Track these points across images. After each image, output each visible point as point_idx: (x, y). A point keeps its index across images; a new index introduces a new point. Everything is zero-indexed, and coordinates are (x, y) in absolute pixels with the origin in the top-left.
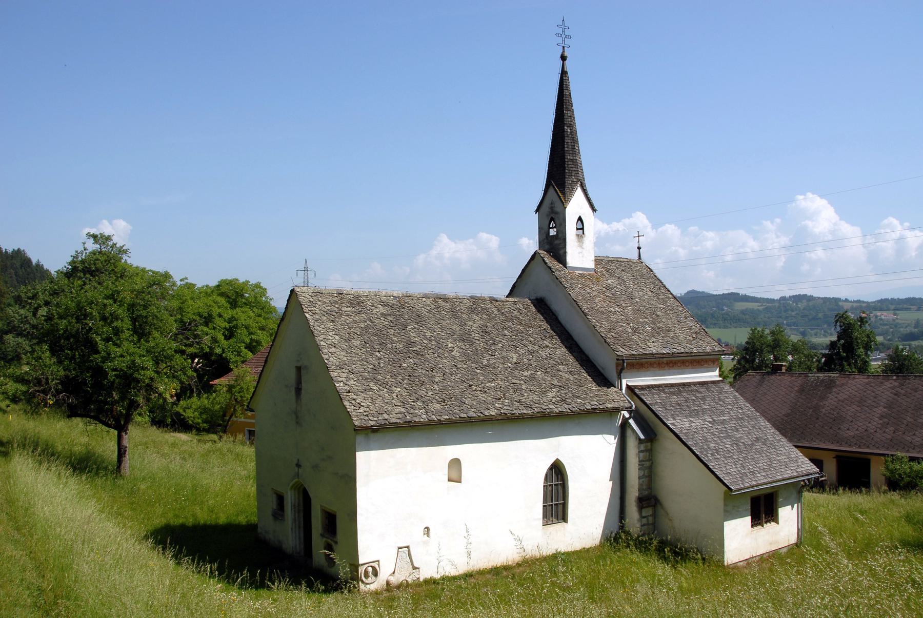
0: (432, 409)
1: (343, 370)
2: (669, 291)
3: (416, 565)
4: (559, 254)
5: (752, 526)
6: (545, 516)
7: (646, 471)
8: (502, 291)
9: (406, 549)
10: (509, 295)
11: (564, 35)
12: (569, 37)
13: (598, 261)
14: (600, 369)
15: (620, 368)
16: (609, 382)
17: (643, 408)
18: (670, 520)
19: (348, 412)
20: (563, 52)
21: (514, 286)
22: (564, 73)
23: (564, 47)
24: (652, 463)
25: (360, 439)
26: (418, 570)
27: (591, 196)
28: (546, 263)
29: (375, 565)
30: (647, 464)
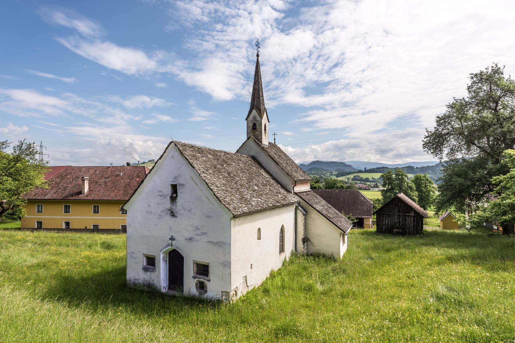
8: (234, 151)
18: (314, 246)
20: (258, 53)
23: (258, 51)
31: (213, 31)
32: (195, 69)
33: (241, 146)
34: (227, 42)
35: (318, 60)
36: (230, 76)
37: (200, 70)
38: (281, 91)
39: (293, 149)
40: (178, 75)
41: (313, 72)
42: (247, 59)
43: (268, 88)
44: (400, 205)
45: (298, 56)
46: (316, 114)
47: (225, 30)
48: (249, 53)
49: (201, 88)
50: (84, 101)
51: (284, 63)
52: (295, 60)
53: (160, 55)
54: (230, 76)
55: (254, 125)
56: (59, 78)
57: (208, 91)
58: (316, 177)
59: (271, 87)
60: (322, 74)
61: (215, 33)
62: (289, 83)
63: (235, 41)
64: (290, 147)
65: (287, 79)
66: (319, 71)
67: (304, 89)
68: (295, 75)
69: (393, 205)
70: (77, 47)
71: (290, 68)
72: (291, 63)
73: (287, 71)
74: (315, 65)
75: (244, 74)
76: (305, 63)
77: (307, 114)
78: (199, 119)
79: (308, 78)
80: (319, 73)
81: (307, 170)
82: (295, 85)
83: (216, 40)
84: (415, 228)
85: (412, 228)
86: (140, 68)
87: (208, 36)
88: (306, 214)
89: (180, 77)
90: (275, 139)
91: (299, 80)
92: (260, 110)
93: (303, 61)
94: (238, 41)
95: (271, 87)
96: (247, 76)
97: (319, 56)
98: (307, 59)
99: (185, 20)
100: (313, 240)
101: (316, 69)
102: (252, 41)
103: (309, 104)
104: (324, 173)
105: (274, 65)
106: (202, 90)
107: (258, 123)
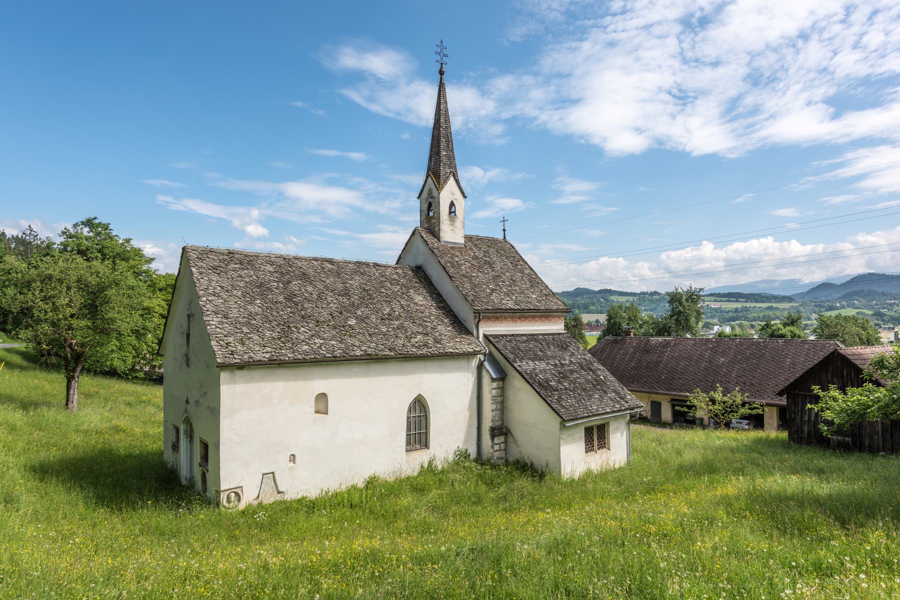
0: (300, 350)
1: (218, 316)
2: (526, 263)
3: (281, 489)
4: (435, 233)
5: (587, 452)
6: (408, 443)
7: (498, 405)
8: (392, 262)
9: (272, 475)
10: (397, 263)
11: (442, 53)
12: (446, 56)
13: (468, 238)
14: (462, 321)
15: (477, 320)
16: (467, 330)
17: (496, 354)
18: (518, 446)
19: (214, 351)
20: (442, 67)
21: (400, 258)
23: (442, 64)
25: (224, 376)
26: (283, 494)
27: (462, 185)
28: (422, 237)
29: (239, 491)
30: (500, 399)
31: (603, 17)
32: (567, 102)
33: (404, 249)
34: (633, 33)
35: (872, 24)
36: (643, 101)
37: (576, 102)
38: (765, 116)
39: (802, 247)
40: (536, 118)
41: (857, 55)
42: (680, 58)
43: (734, 113)
44: (847, 374)
45: (813, 27)
46: (866, 157)
47: (629, 9)
48: (685, 45)
49: (582, 137)
50: (380, 189)
51: (775, 50)
52: (804, 36)
53: (504, 84)
54: (643, 101)
55: (430, 205)
56: (345, 154)
57: (596, 141)
58: (864, 314)
59: (741, 110)
60: (883, 56)
61: (608, 19)
62: (789, 92)
63: (651, 25)
64: (794, 242)
65: (781, 85)
66: (875, 51)
67: (828, 101)
68: (803, 72)
69: (829, 374)
70: (371, 99)
71: (789, 58)
72: (794, 46)
73: (783, 66)
74: (861, 38)
75: (675, 91)
76: (830, 39)
77: (839, 160)
78: (574, 199)
79: (840, 73)
80: (874, 54)
81: (840, 298)
82: (804, 96)
83: (611, 32)
84: (888, 437)
85: (880, 435)
86: (468, 117)
87: (595, 29)
88: (502, 377)
89: (539, 122)
90: (504, 230)
91: (817, 82)
92: (439, 176)
93: (826, 35)
94: (660, 23)
95: (741, 110)
96: (682, 95)
97: (875, 13)
98: (837, 28)
99: (548, 8)
100: (519, 432)
101: (865, 47)
102: (692, 15)
103: (847, 135)
104: (891, 305)
105: (748, 58)
106: (583, 141)
107: (435, 202)
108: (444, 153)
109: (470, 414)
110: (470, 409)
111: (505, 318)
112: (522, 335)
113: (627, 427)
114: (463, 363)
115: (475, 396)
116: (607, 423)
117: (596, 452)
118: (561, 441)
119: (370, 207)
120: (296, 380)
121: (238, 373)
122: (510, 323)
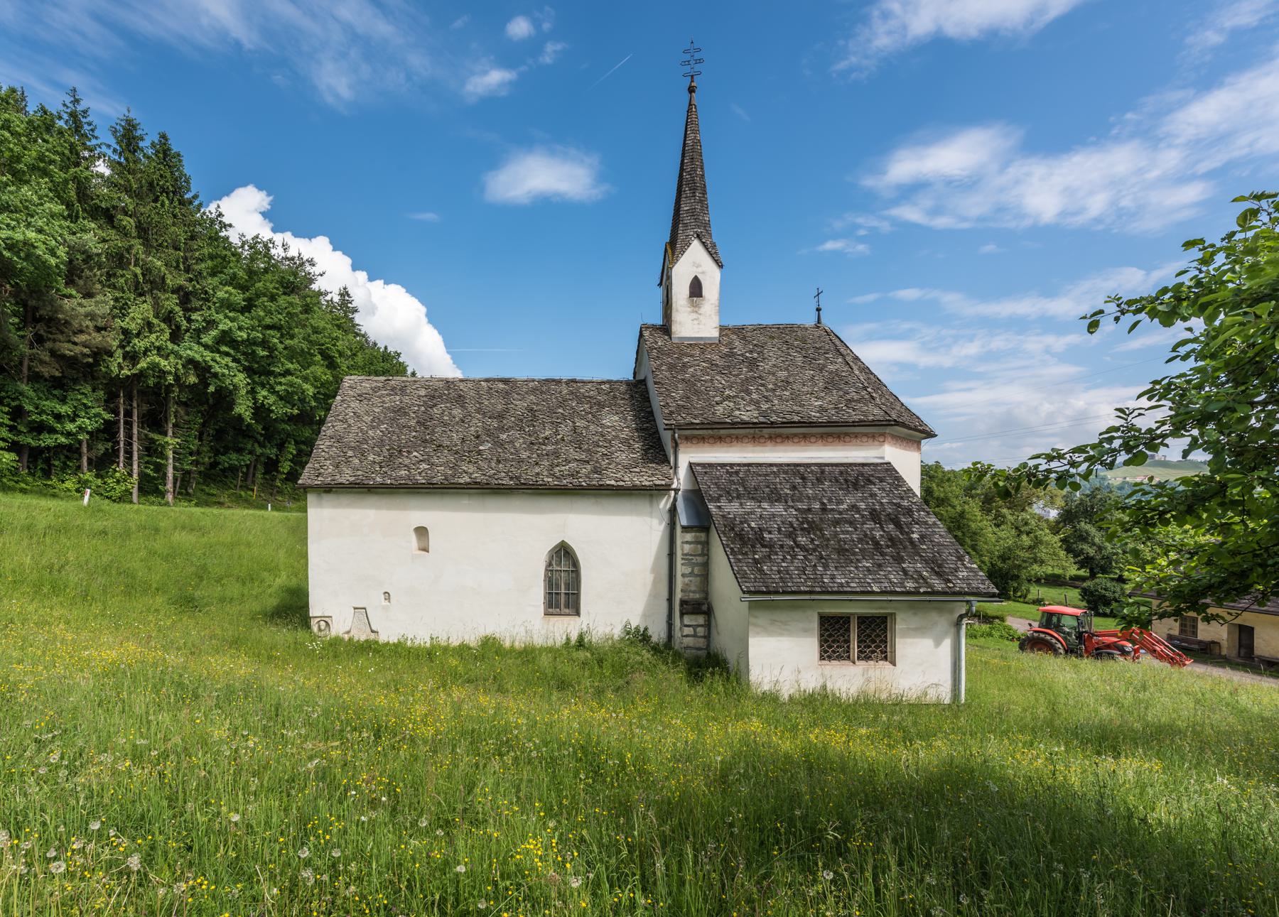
5: (822, 658)
11: (693, 57)
13: (722, 329)
22: (690, 122)
24: (708, 559)
33: (637, 359)
90: (819, 310)
108: (686, 209)
109: (655, 578)
110: (654, 569)
111: (737, 438)
112: (771, 465)
113: (953, 630)
114: (643, 504)
115: (666, 551)
116: (891, 614)
117: (854, 663)
118: (750, 628)
119: (928, 360)
120: (389, 509)
121: (325, 496)
122: (750, 447)
